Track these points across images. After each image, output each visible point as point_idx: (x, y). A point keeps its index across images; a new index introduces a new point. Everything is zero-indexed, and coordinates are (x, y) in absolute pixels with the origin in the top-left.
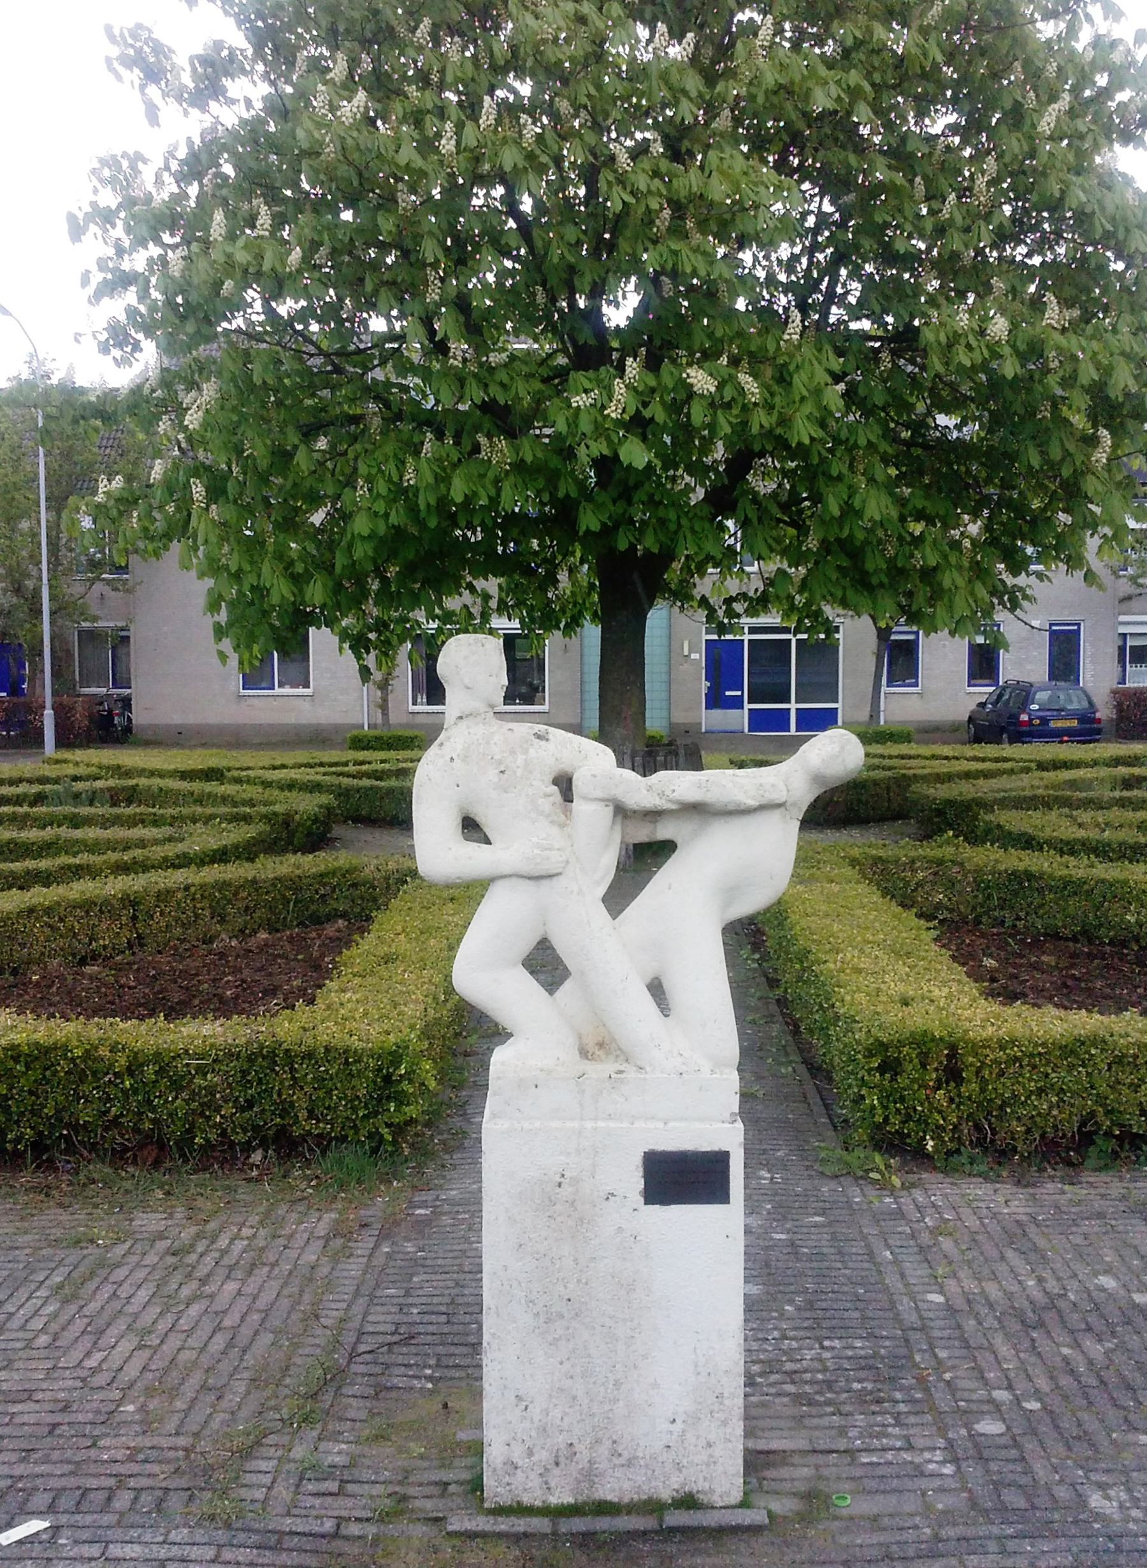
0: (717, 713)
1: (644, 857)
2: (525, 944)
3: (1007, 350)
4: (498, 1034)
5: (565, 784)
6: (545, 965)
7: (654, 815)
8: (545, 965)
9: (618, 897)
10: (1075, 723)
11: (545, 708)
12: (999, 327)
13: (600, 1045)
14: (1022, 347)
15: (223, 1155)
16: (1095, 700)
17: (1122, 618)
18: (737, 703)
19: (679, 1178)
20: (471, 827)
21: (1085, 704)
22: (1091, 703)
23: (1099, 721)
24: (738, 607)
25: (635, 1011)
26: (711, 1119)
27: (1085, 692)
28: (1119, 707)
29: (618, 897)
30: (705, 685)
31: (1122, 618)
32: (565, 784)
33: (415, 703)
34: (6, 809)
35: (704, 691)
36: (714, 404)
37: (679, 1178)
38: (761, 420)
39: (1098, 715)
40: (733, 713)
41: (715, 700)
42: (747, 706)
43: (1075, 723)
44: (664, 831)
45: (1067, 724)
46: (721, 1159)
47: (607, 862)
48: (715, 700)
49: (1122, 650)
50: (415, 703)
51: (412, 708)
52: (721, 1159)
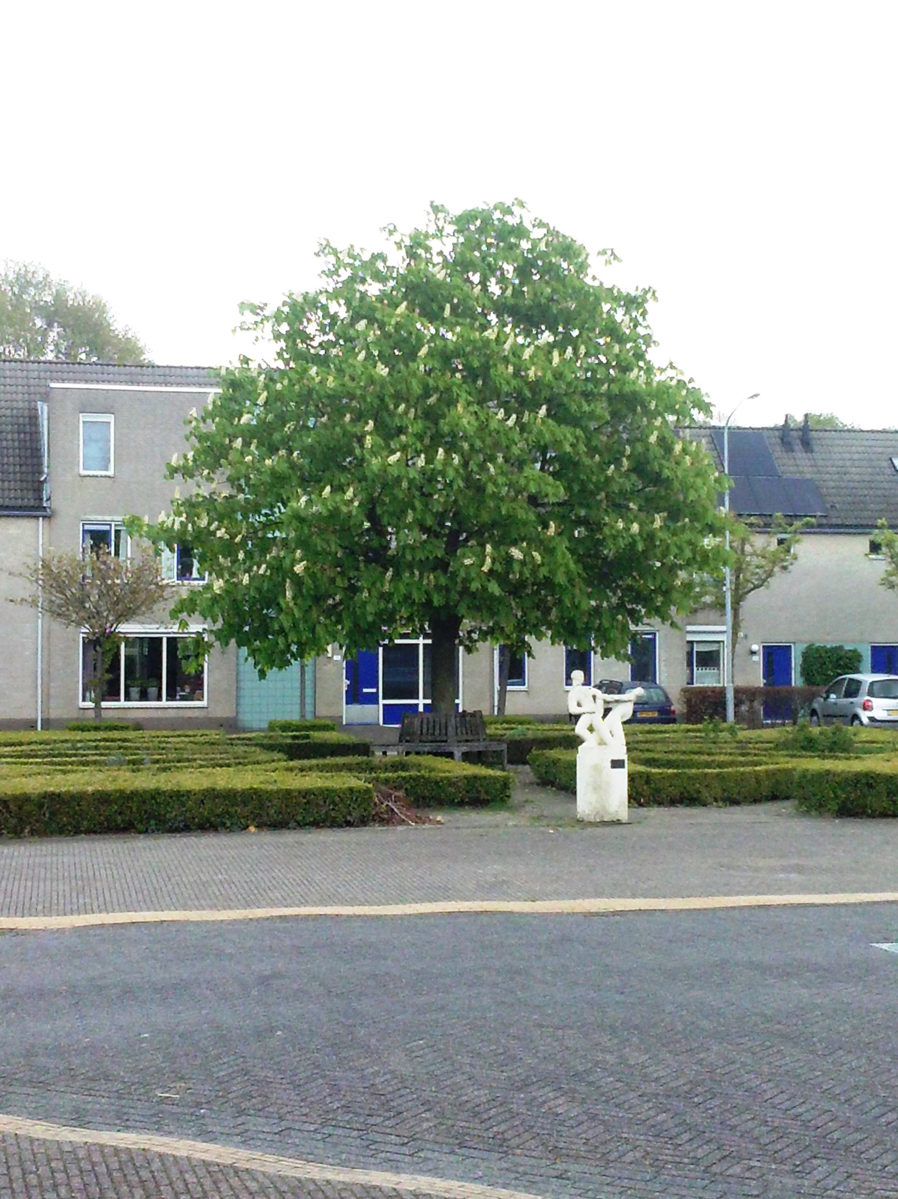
0: (356, 708)
1: (607, 711)
2: (588, 725)
3: (638, 538)
4: (582, 742)
5: (594, 697)
6: (591, 729)
7: (609, 702)
8: (591, 729)
9: (604, 716)
10: (656, 715)
11: (204, 703)
12: (635, 527)
13: (602, 743)
14: (645, 536)
15: (461, 804)
16: (670, 696)
17: (690, 628)
18: (372, 699)
19: (617, 764)
20: (579, 705)
21: (663, 699)
22: (667, 698)
23: (674, 712)
24: (475, 636)
25: (607, 737)
26: (623, 755)
27: (661, 688)
28: (688, 702)
29: (604, 716)
30: (346, 682)
31: (690, 628)
32: (594, 697)
33: (84, 700)
34: (4, 760)
35: (345, 689)
36: (523, 563)
37: (617, 764)
38: (543, 572)
39: (673, 708)
40: (369, 708)
41: (354, 696)
42: (382, 702)
43: (656, 715)
44: (610, 706)
45: (650, 715)
46: (623, 761)
47: (602, 711)
48: (354, 696)
49: (690, 654)
50: (84, 700)
51: (82, 704)
52: (623, 761)
